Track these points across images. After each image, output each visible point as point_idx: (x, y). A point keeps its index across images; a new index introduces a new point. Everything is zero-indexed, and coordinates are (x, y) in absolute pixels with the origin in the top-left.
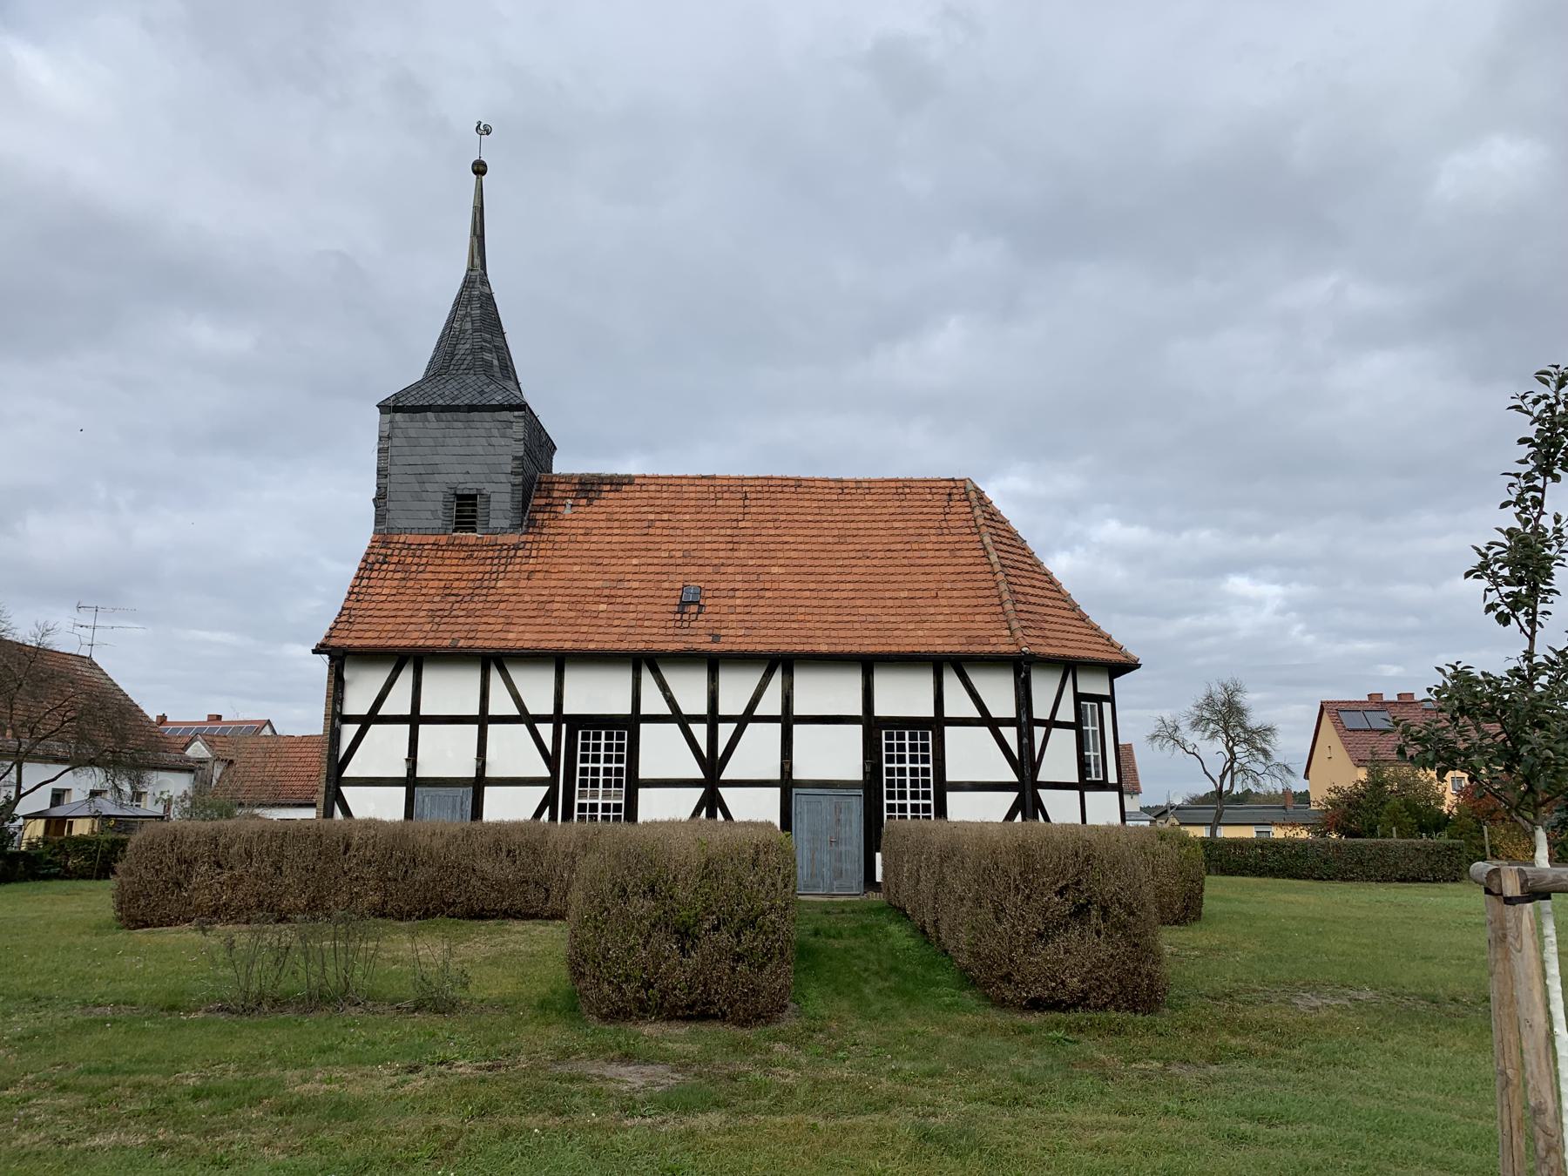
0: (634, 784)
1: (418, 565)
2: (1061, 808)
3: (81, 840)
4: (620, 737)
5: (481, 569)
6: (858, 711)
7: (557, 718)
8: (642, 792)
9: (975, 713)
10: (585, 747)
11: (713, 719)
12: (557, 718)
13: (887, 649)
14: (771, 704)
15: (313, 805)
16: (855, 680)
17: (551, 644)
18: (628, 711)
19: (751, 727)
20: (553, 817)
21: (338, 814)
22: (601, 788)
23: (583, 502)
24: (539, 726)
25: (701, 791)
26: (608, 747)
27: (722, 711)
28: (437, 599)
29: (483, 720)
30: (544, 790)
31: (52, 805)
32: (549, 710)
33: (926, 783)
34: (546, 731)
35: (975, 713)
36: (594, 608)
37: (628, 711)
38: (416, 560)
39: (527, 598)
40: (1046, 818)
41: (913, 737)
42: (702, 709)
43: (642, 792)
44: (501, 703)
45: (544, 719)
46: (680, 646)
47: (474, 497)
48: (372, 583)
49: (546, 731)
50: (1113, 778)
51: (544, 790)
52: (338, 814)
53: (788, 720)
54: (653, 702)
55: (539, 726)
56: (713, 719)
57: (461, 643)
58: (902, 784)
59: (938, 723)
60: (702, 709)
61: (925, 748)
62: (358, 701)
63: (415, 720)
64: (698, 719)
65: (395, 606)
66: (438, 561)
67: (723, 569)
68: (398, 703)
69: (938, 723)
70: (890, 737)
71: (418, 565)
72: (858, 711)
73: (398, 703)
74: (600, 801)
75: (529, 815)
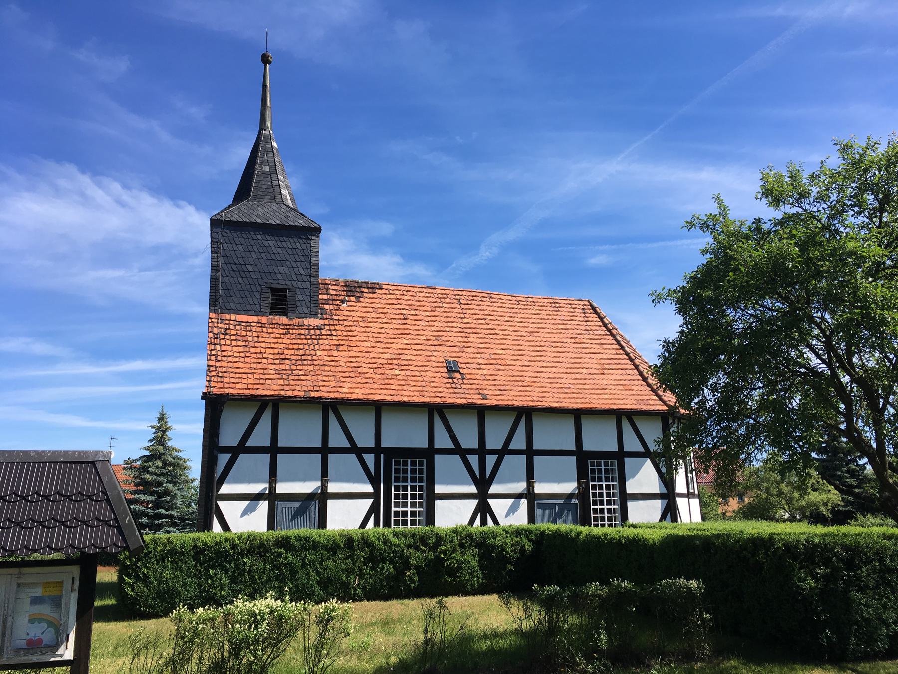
0: (625, 498)
1: (253, 337)
2: (690, 513)
3: (349, 543)
4: (421, 464)
5: (300, 342)
6: (573, 447)
7: (377, 450)
8: (438, 503)
9: (250, 443)
10: (397, 471)
11: (482, 451)
12: (377, 450)
13: (541, 404)
14: (518, 442)
15: (704, 518)
16: (569, 426)
17: (376, 395)
18: (425, 445)
19: (507, 458)
20: (377, 524)
21: (490, 522)
22: (409, 500)
23: (353, 299)
24: (365, 456)
25: (477, 501)
26: (413, 471)
27: (488, 447)
28: (277, 362)
29: (325, 451)
30: (369, 502)
31: (661, 520)
32: (371, 444)
33: (594, 495)
34: (370, 459)
35: (250, 443)
36: (392, 372)
37: (425, 445)
38: (249, 333)
39: (343, 364)
40: (496, 522)
41: (413, 464)
42: (475, 445)
43: (438, 503)
44: (337, 439)
45: (368, 450)
46: (465, 401)
47: (285, 290)
48: (223, 348)
49: (370, 459)
50: (697, 492)
51: (369, 502)
52: (490, 522)
53: (530, 453)
54: (442, 440)
55: (365, 456)
56: (482, 451)
57: (313, 394)
58: (601, 495)
59: (620, 455)
60: (475, 445)
61: (421, 471)
62: (229, 436)
63: (274, 450)
64: (472, 452)
65: (248, 366)
66: (266, 335)
67: (466, 350)
68: (518, 442)
69: (620, 455)
70: (397, 463)
71: (253, 337)
72: (573, 447)
73: (261, 437)
74: (409, 509)
75: (466, 522)
